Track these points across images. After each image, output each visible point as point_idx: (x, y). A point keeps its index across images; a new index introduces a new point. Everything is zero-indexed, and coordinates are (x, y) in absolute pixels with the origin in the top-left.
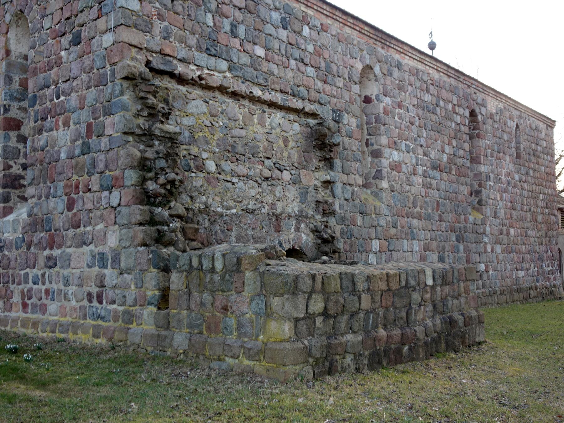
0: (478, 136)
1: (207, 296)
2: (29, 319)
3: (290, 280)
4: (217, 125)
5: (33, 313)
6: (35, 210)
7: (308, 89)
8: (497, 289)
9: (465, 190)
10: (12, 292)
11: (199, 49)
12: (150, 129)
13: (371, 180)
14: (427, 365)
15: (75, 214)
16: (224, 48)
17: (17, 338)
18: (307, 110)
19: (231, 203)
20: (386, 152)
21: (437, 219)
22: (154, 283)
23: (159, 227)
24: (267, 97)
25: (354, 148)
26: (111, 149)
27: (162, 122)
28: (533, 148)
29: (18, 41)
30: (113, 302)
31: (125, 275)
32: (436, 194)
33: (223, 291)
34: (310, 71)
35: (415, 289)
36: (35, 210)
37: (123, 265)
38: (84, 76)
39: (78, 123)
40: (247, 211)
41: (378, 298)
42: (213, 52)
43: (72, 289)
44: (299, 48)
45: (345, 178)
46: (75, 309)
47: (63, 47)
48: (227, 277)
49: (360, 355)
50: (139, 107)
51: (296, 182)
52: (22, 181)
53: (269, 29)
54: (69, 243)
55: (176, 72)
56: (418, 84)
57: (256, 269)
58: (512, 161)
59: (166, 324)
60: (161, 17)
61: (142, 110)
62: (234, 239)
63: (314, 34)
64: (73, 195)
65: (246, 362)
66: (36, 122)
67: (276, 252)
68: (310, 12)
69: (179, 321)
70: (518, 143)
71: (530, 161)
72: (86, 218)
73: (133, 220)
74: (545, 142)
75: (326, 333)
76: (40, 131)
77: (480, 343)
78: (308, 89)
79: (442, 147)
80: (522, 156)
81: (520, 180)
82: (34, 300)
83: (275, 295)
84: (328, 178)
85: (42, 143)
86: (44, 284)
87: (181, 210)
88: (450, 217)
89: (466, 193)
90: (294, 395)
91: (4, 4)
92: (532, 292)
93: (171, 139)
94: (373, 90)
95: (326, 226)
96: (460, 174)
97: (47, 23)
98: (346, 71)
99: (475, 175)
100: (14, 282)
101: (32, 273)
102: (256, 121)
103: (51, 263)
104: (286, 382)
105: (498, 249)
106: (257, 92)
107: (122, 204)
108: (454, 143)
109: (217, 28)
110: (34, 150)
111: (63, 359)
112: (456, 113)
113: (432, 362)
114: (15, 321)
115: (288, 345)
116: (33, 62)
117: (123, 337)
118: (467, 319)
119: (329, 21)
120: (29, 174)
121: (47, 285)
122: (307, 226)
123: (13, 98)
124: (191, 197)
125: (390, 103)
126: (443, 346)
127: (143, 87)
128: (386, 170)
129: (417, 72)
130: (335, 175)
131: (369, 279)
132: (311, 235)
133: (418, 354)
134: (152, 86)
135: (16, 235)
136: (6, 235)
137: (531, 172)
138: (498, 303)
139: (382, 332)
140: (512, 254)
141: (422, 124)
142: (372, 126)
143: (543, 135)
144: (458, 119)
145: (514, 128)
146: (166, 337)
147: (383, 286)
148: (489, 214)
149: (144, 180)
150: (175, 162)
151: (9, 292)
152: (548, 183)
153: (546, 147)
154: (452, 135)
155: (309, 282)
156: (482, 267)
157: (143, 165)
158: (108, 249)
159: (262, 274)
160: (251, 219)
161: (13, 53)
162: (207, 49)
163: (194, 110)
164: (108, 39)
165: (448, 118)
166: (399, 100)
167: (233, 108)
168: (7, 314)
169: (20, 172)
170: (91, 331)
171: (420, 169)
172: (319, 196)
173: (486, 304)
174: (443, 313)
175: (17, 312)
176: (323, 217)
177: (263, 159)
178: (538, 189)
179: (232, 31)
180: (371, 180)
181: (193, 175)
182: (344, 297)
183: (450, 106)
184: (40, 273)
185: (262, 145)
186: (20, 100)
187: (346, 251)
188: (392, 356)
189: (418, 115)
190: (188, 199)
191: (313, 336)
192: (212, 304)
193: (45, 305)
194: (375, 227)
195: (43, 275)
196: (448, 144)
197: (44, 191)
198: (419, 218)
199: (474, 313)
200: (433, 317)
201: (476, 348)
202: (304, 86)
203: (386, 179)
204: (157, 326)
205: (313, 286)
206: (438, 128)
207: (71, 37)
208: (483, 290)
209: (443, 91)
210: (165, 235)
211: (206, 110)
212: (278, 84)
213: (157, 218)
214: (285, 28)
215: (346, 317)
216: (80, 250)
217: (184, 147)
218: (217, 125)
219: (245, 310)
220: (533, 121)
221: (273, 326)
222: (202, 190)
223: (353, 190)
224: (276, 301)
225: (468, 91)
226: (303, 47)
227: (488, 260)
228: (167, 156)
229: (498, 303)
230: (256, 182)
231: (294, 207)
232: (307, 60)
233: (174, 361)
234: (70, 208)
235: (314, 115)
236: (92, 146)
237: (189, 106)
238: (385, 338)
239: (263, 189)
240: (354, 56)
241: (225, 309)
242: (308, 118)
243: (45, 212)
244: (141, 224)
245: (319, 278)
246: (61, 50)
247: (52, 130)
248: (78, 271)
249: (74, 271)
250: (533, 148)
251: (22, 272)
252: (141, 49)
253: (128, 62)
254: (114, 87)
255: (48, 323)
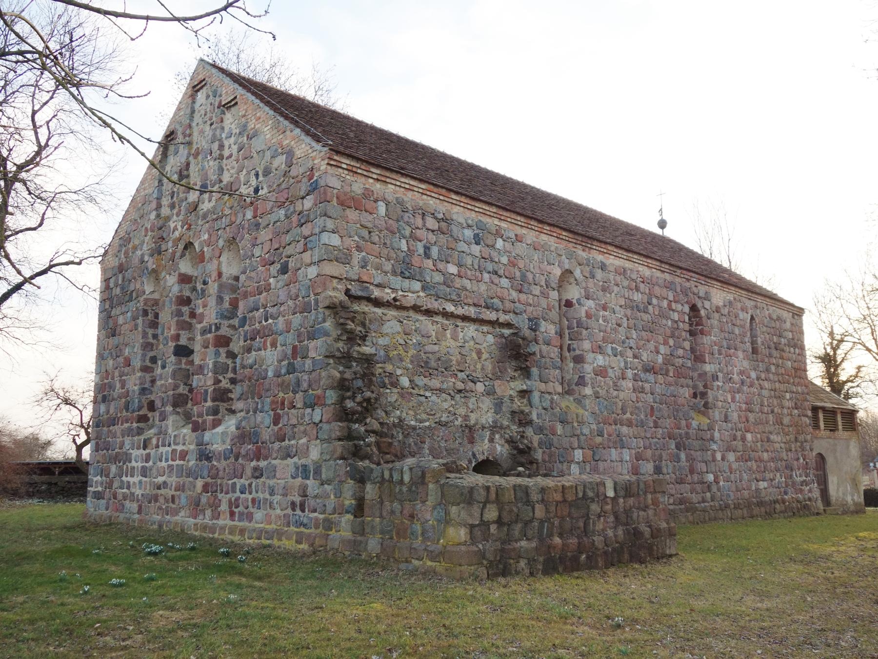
0: (702, 332)
1: (396, 505)
2: (236, 527)
3: (466, 491)
4: (411, 343)
5: (239, 521)
6: (243, 424)
7: (502, 300)
8: (730, 502)
9: (686, 393)
10: (220, 500)
11: (394, 273)
12: (348, 352)
13: (574, 387)
14: (605, 573)
15: (281, 429)
16: (418, 270)
17: (225, 544)
18: (501, 320)
19: (424, 416)
20: (590, 357)
21: (652, 425)
22: (351, 493)
23: (356, 442)
24: (460, 311)
25: (552, 355)
26: (314, 370)
27: (360, 345)
28: (775, 340)
29: (229, 264)
30: (315, 511)
31: (326, 486)
32: (650, 399)
33: (410, 501)
34: (505, 282)
35: (593, 500)
36: (243, 424)
37: (324, 476)
38: (290, 303)
39: (285, 345)
40: (439, 423)
41: (553, 509)
42: (407, 274)
43: (277, 498)
44: (492, 261)
45: (542, 387)
46: (280, 517)
47: (272, 275)
48: (414, 488)
49: (534, 560)
50: (339, 332)
51: (490, 392)
52: (230, 395)
53: (462, 246)
54: (275, 455)
55: (373, 296)
56: (626, 283)
57: (437, 482)
58: (746, 358)
59: (361, 530)
60: (359, 249)
61: (341, 334)
62: (427, 451)
63: (508, 246)
64: (279, 411)
65: (429, 563)
66: (245, 341)
67: (457, 466)
68: (504, 225)
69: (373, 527)
70: (753, 337)
71: (771, 356)
72: (290, 433)
73: (333, 436)
74: (790, 334)
75: (500, 538)
76: (249, 350)
77: (671, 556)
78: (502, 300)
79: (656, 347)
80: (760, 350)
81: (758, 379)
82: (241, 508)
83: (453, 505)
84: (525, 387)
85: (250, 361)
86: (250, 493)
87: (376, 426)
88: (668, 423)
89: (687, 396)
90: (466, 589)
91: (218, 230)
92: (777, 506)
93: (368, 360)
94: (573, 293)
95: (522, 437)
96: (679, 375)
97: (257, 252)
98: (543, 278)
99: (700, 375)
100: (222, 492)
101: (239, 482)
102: (449, 336)
103: (258, 473)
104: (461, 579)
105: (731, 457)
106: (450, 308)
107: (324, 420)
108: (671, 342)
109: (411, 252)
110: (244, 367)
111: (271, 561)
112: (673, 310)
113: (611, 571)
114: (222, 528)
115: (463, 548)
116: (243, 286)
117: (323, 542)
118: (655, 531)
119: (524, 231)
120: (238, 390)
121: (254, 495)
122: (501, 436)
123: (223, 317)
124: (386, 412)
125: (593, 306)
126: (626, 556)
127: (343, 314)
128: (589, 376)
129: (625, 271)
130: (534, 384)
131: (543, 490)
132: (507, 446)
133: (597, 562)
134: (350, 315)
135: (224, 447)
136: (215, 446)
137: (773, 368)
138: (732, 519)
139: (557, 540)
140: (749, 463)
141: (631, 325)
142: (572, 329)
143: (788, 325)
144: (676, 316)
145: (749, 321)
146: (361, 542)
147: (558, 497)
148: (717, 417)
149: (342, 399)
150: (371, 381)
151: (217, 501)
152: (797, 380)
153: (793, 339)
154: (669, 332)
155: (483, 493)
156: (711, 477)
157: (342, 386)
158: (310, 461)
159: (442, 486)
160: (444, 432)
161: (224, 275)
162: (402, 272)
163: (389, 331)
164: (312, 272)
165: (663, 315)
166: (603, 302)
167: (426, 324)
168: (215, 522)
169: (228, 386)
170: (294, 537)
171: (629, 373)
172: (514, 405)
173: (715, 519)
174: (627, 524)
175: (225, 520)
176: (519, 427)
177: (456, 372)
178: (782, 387)
179: (425, 252)
180: (574, 387)
181: (388, 391)
182: (518, 507)
183: (665, 304)
184: (247, 483)
185: (455, 359)
186: (230, 318)
187: (544, 461)
188: (568, 563)
189: (626, 316)
190: (383, 414)
191: (488, 541)
192: (401, 512)
193: (252, 513)
194: (578, 436)
195: (250, 485)
196: (664, 344)
197: (252, 406)
198: (630, 424)
199: (664, 525)
200: (615, 528)
201: (665, 560)
202: (498, 297)
203: (589, 386)
204: (354, 533)
205: (488, 497)
206: (650, 329)
207: (279, 266)
208: (712, 504)
209: (656, 288)
210: (361, 449)
211: (400, 330)
212: (471, 298)
213: (355, 434)
214: (477, 243)
215: (520, 525)
216: (285, 462)
217: (380, 365)
218: (411, 343)
219: (428, 518)
220: (774, 311)
221: (451, 531)
222: (396, 405)
223: (552, 399)
224: (454, 510)
225: (687, 284)
226: (496, 260)
227: (717, 469)
228: (364, 376)
229: (732, 519)
230: (449, 394)
231: (488, 418)
232: (501, 272)
233: (367, 563)
234: (276, 423)
235: (508, 325)
236: (296, 366)
237: (385, 327)
238: (560, 546)
239: (456, 401)
240: (552, 262)
241: (412, 516)
242: (503, 328)
243: (253, 425)
244: (340, 439)
245: (493, 490)
246: (270, 278)
247: (261, 350)
248: (283, 481)
249: (279, 481)
250: (775, 340)
251: (230, 482)
252: (341, 279)
253: (330, 293)
254: (317, 314)
255: (254, 530)
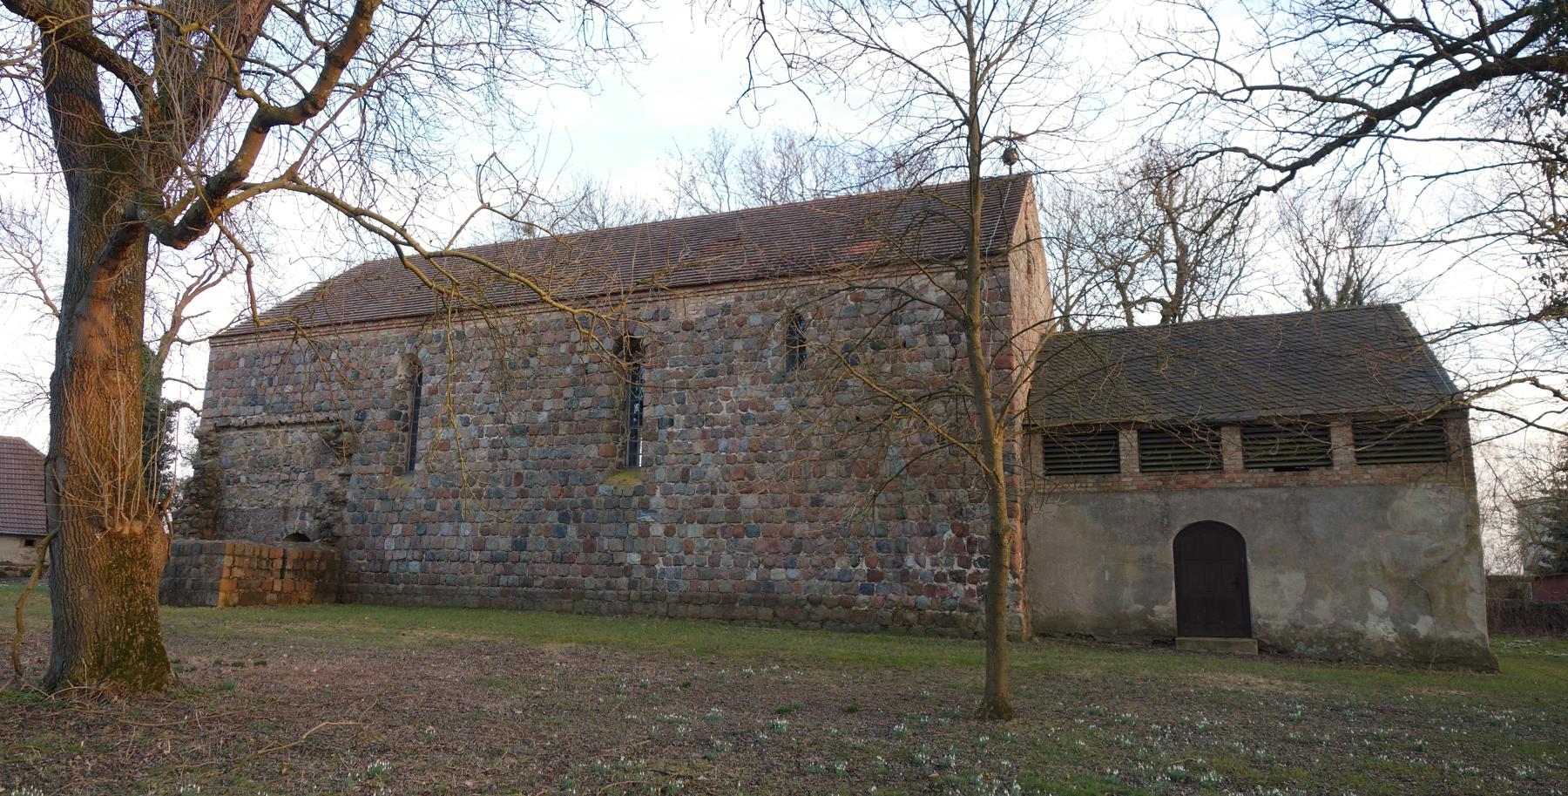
51: (308, 480)
106: (285, 419)
156: (635, 558)
235: (329, 421)
